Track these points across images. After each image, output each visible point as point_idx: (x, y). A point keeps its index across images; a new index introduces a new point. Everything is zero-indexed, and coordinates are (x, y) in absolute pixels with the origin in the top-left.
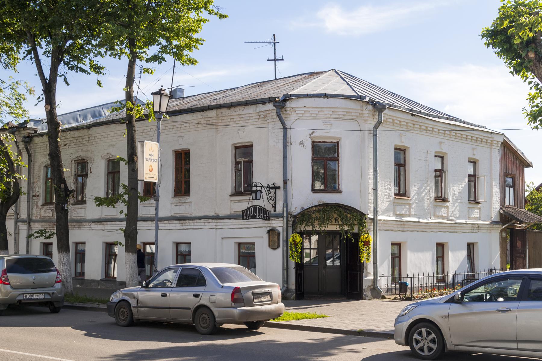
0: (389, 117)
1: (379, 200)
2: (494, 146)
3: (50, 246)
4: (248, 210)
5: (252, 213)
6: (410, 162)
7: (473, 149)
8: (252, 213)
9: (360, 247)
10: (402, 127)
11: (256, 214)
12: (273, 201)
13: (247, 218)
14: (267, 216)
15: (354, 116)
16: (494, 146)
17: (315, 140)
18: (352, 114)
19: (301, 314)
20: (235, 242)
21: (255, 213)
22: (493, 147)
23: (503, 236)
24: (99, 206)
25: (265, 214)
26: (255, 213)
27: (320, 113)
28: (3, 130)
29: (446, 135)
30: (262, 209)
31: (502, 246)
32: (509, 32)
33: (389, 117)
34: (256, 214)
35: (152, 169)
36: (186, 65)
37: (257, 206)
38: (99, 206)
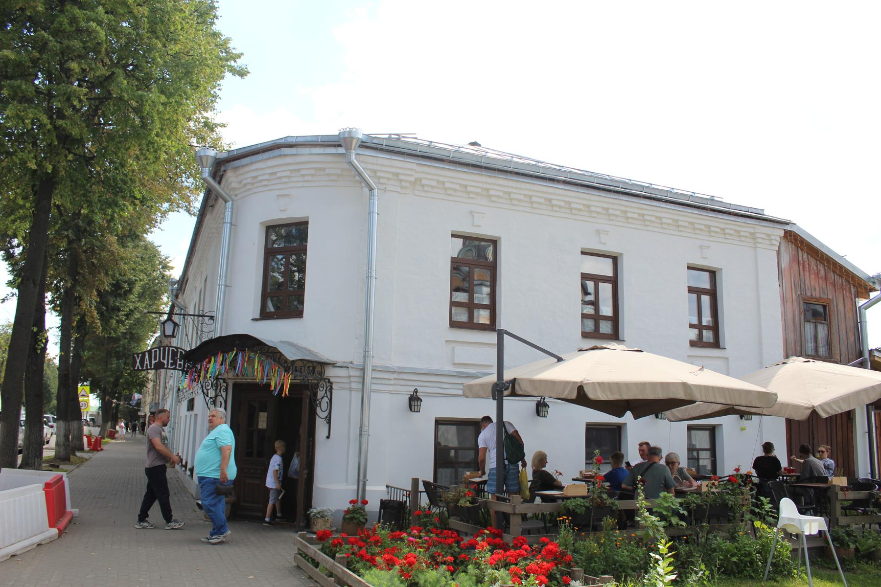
2: (760, 243)
4: (147, 353)
5: (155, 359)
8: (155, 359)
9: (44, 114)
11: (165, 362)
13: (142, 366)
16: (760, 243)
21: (164, 359)
22: (758, 245)
26: (164, 359)
28: (870, 556)
30: (181, 352)
34: (165, 362)
36: (6, 295)
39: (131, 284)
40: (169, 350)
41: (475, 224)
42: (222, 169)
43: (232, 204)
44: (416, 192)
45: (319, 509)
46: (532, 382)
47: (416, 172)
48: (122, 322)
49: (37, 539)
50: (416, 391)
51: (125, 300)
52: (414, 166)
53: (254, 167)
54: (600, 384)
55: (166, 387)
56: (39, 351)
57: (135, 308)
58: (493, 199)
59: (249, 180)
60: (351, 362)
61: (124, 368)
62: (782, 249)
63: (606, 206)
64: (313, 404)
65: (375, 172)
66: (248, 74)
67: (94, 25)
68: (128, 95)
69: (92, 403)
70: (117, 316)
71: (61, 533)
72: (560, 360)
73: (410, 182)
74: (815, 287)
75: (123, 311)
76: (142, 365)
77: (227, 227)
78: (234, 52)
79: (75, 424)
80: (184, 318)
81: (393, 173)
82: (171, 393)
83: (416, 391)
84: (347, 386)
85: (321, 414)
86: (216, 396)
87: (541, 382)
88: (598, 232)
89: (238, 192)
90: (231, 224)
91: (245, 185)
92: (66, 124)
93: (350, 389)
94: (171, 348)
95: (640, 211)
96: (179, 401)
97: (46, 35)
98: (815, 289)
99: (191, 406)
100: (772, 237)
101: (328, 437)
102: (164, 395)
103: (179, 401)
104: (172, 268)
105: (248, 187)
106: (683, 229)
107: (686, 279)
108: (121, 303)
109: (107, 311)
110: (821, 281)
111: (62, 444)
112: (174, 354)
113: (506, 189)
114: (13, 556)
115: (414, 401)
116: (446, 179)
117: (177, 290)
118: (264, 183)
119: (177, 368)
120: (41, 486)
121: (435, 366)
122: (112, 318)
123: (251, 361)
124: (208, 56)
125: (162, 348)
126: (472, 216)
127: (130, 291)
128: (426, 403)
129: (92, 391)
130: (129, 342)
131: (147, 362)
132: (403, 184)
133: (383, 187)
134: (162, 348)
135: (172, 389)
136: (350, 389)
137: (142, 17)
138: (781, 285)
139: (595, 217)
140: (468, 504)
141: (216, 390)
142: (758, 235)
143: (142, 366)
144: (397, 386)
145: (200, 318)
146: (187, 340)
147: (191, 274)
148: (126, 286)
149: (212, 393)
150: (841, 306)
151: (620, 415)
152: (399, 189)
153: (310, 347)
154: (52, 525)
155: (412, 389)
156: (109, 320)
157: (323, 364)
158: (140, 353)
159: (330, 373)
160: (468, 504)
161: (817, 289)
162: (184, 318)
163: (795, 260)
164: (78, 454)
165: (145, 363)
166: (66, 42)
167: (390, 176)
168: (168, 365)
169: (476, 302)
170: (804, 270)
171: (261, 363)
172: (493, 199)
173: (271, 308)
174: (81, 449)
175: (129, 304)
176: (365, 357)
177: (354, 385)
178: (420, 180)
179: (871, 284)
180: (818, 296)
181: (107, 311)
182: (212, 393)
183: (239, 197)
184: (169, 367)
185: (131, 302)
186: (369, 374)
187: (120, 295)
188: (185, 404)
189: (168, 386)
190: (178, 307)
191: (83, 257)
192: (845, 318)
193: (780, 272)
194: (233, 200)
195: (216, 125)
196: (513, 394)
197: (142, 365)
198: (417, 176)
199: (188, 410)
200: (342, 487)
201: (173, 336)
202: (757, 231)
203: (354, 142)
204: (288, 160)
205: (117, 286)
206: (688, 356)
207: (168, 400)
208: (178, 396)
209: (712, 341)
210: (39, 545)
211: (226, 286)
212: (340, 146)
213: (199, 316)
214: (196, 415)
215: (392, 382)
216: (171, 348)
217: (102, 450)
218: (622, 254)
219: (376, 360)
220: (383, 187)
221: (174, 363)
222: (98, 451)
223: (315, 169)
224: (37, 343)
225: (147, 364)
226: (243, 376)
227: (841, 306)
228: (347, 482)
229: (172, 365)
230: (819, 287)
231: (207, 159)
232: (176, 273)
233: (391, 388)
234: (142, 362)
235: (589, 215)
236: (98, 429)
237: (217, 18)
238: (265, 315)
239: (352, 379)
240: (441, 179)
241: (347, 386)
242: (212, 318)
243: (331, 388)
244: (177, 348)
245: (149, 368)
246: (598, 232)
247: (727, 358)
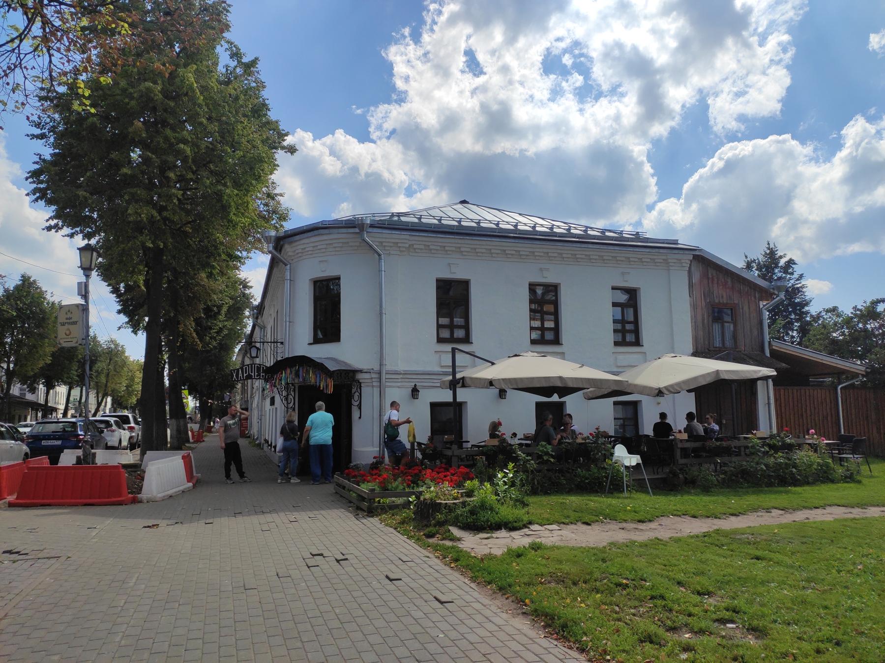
5: (246, 373)
7: (623, 274)
8: (246, 373)
13: (238, 379)
19: (603, 573)
21: (252, 372)
22: (671, 268)
24: (37, 202)
26: (252, 372)
30: (263, 368)
32: (41, 388)
34: (253, 374)
35: (70, 333)
38: (37, 202)
39: (220, 307)
42: (282, 243)
43: (290, 267)
44: (411, 254)
45: (355, 463)
46: (471, 378)
47: (409, 240)
48: (215, 338)
49: (182, 488)
50: (415, 385)
51: (215, 320)
52: (408, 237)
53: (302, 242)
54: (503, 380)
55: (253, 388)
56: (160, 370)
57: (224, 326)
58: (464, 253)
59: (300, 251)
60: (373, 369)
61: (216, 373)
62: (693, 268)
63: (545, 251)
64: (350, 397)
65: (381, 243)
66: (297, 152)
67: (182, 146)
68: (211, 189)
69: (191, 403)
70: (210, 334)
71: (194, 486)
72: (493, 364)
73: (406, 248)
74: (721, 294)
75: (214, 329)
76: (237, 378)
77: (287, 284)
78: (283, 132)
79: (182, 422)
80: (263, 344)
81: (394, 243)
82: (257, 392)
83: (415, 385)
84: (371, 384)
85: (355, 403)
86: (288, 395)
87: (477, 379)
88: (541, 270)
89: (293, 258)
90: (290, 280)
91: (298, 253)
92: (169, 214)
93: (373, 386)
95: (572, 252)
96: (264, 398)
97: (150, 154)
98: (722, 297)
99: (272, 403)
100: (683, 261)
101: (360, 418)
102: (252, 394)
103: (264, 398)
104: (251, 287)
105: (300, 255)
106: (608, 262)
108: (212, 323)
109: (202, 329)
110: (728, 290)
111: (175, 436)
112: (259, 369)
113: (473, 246)
114: (170, 496)
115: (415, 392)
116: (430, 244)
117: (257, 314)
118: (310, 253)
120: (181, 457)
121: (429, 368)
122: (206, 336)
123: (308, 372)
124: (264, 155)
126: (450, 266)
127: (219, 313)
128: (422, 393)
129: (190, 394)
130: (219, 351)
132: (401, 249)
133: (388, 252)
135: (258, 389)
136: (373, 386)
137: (215, 132)
138: (691, 296)
139: (538, 259)
140: (431, 452)
141: (287, 391)
142: (670, 261)
145: (275, 344)
146: (268, 360)
147: (266, 304)
148: (215, 309)
149: (284, 393)
150: (746, 308)
151: (550, 396)
152: (399, 253)
153: (346, 361)
154: (188, 481)
155: (413, 384)
156: (203, 338)
157: (355, 372)
159: (360, 376)
160: (431, 452)
161: (725, 296)
162: (263, 344)
163: (705, 276)
164: (187, 445)
166: (164, 157)
167: (392, 245)
169: (620, 318)
170: (712, 283)
171: (314, 373)
172: (464, 253)
173: (320, 336)
174: (188, 441)
175: (219, 323)
176: (380, 365)
177: (375, 384)
178: (413, 245)
179: (771, 290)
180: (725, 302)
181: (202, 329)
182: (284, 393)
183: (294, 261)
185: (220, 321)
186: (384, 376)
187: (211, 317)
188: (268, 401)
189: (255, 386)
190: (259, 326)
191: (181, 292)
192: (750, 317)
193: (691, 286)
194: (290, 264)
195: (276, 195)
196: (463, 386)
197: (237, 378)
198: (410, 243)
199: (271, 405)
200: (370, 449)
201: (257, 357)
202: (669, 257)
203: (365, 225)
204: (325, 237)
205: (208, 310)
207: (255, 398)
208: (263, 395)
209: (634, 341)
210: (183, 492)
211: (290, 322)
212: (355, 227)
213: (274, 342)
214: (276, 408)
215: (400, 380)
217: (204, 441)
218: (560, 284)
219: (389, 366)
220: (388, 252)
221: (259, 375)
222: (201, 442)
223: (343, 243)
224: (158, 364)
227: (746, 308)
228: (373, 446)
229: (257, 376)
230: (727, 295)
231: (271, 239)
232: (256, 301)
233: (399, 384)
234: (237, 376)
236: (198, 426)
237: (269, 110)
238: (316, 341)
239: (373, 380)
240: (427, 243)
241: (371, 384)
242: (282, 343)
243: (361, 386)
244: (260, 365)
246: (541, 270)
247: (645, 353)
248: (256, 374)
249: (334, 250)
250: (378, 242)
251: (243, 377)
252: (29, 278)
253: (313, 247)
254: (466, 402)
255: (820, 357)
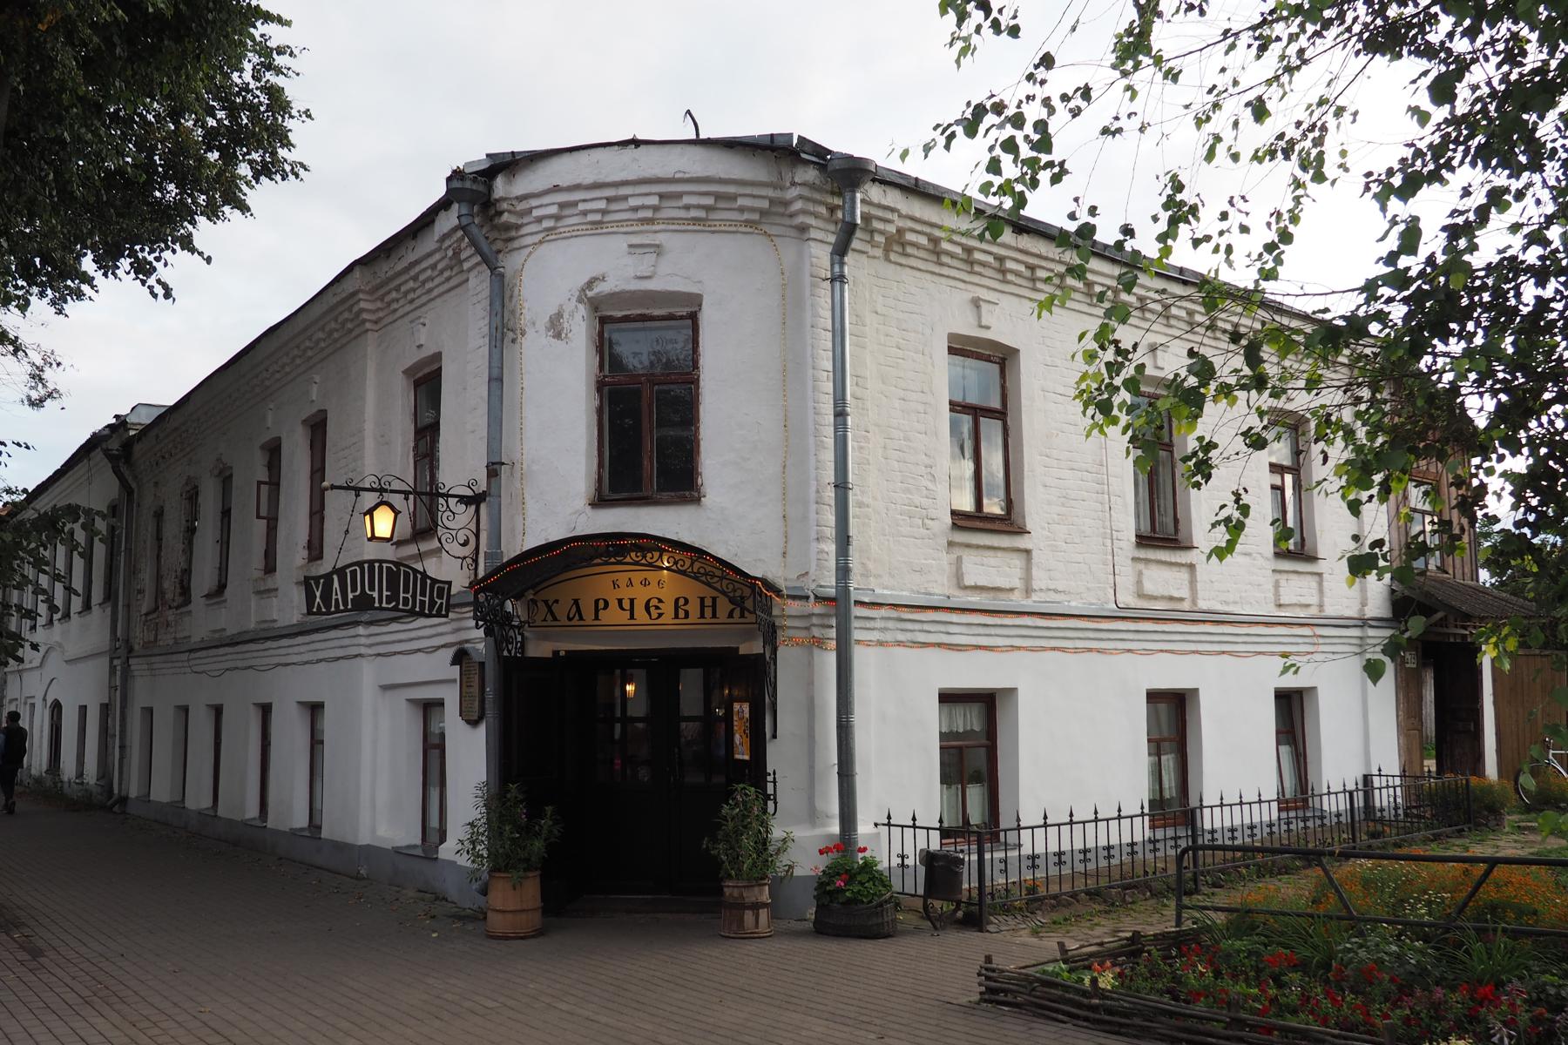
0: (910, 224)
1: (483, 432)
3: (435, 711)
4: (335, 577)
5: (354, 589)
6: (1024, 402)
8: (354, 589)
10: (980, 274)
11: (375, 595)
12: (465, 544)
14: (432, 603)
15: (752, 210)
17: (609, 313)
18: (741, 202)
20: (408, 700)
21: (372, 588)
23: (1408, 666)
25: (423, 594)
26: (372, 588)
27: (614, 207)
29: (1173, 322)
30: (407, 575)
31: (1407, 696)
33: (910, 224)
34: (375, 595)
37: (381, 562)
40: (381, 568)
41: (983, 324)
44: (893, 257)
94: (385, 565)
107: (99, 288)
113: (1031, 260)
119: (401, 606)
125: (366, 566)
126: (978, 307)
131: (336, 594)
134: (366, 566)
143: (328, 606)
144: (1011, 624)
158: (321, 577)
165: (334, 597)
168: (381, 601)
184: (384, 605)
198: (901, 223)
206: (1273, 571)
216: (385, 565)
225: (337, 600)
226: (570, 619)
235: (969, 269)
245: (342, 607)
246: (976, 303)
248: (385, 593)
249: (682, 214)
250: (1185, 309)
251: (345, 603)
252: (58, 304)
253: (609, 200)
254: (1313, 689)
255: (46, 500)
